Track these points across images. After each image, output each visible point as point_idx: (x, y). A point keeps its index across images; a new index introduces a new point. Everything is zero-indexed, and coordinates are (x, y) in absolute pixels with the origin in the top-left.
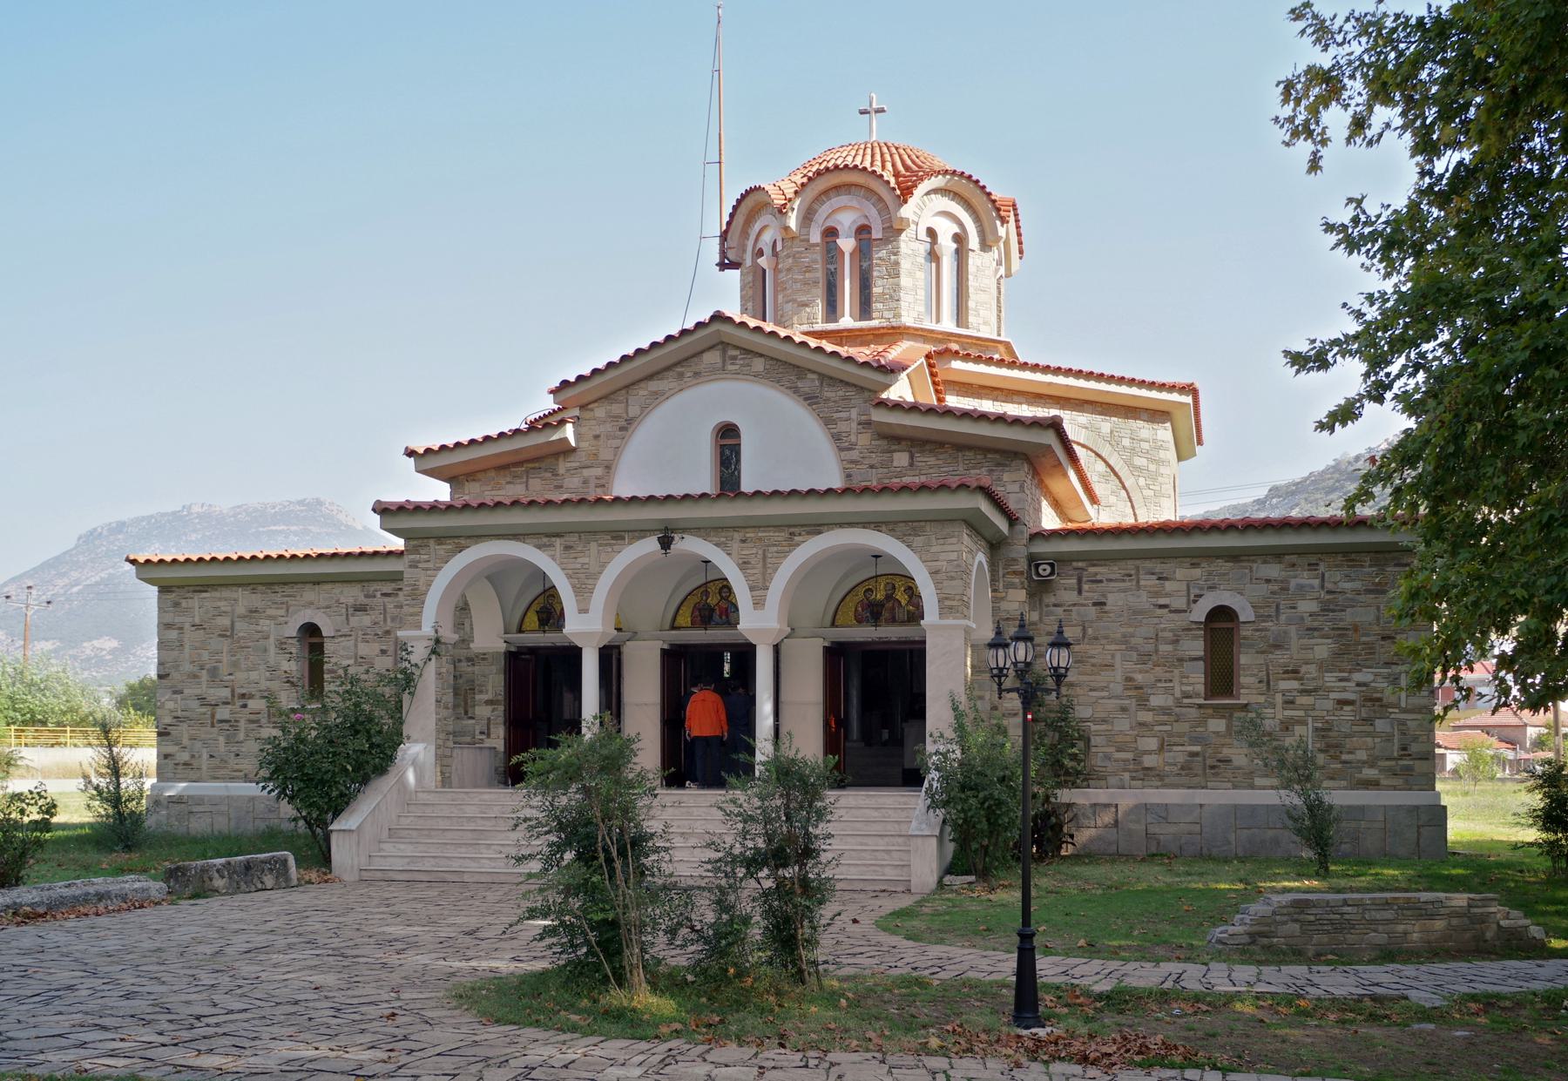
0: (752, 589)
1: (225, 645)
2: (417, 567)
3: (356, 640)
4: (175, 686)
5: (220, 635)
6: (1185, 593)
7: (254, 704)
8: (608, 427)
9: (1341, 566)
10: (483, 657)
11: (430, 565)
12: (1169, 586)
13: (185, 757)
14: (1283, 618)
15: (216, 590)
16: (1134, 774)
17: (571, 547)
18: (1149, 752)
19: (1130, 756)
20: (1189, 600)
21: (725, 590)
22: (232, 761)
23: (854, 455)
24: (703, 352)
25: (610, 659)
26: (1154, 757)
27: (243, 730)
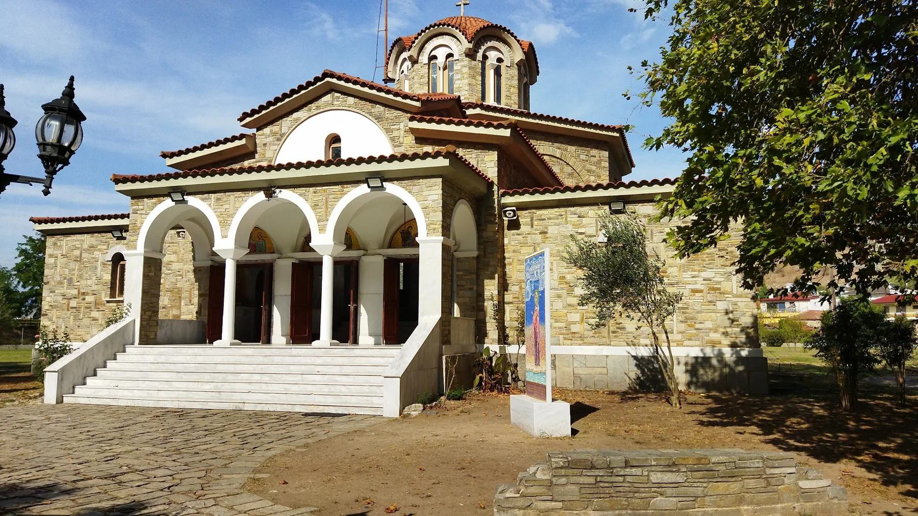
1: (77, 266)
5: (75, 261)
6: (595, 225)
7: (89, 299)
8: (271, 139)
16: (565, 336)
18: (575, 323)
19: (563, 325)
20: (597, 229)
26: (578, 325)
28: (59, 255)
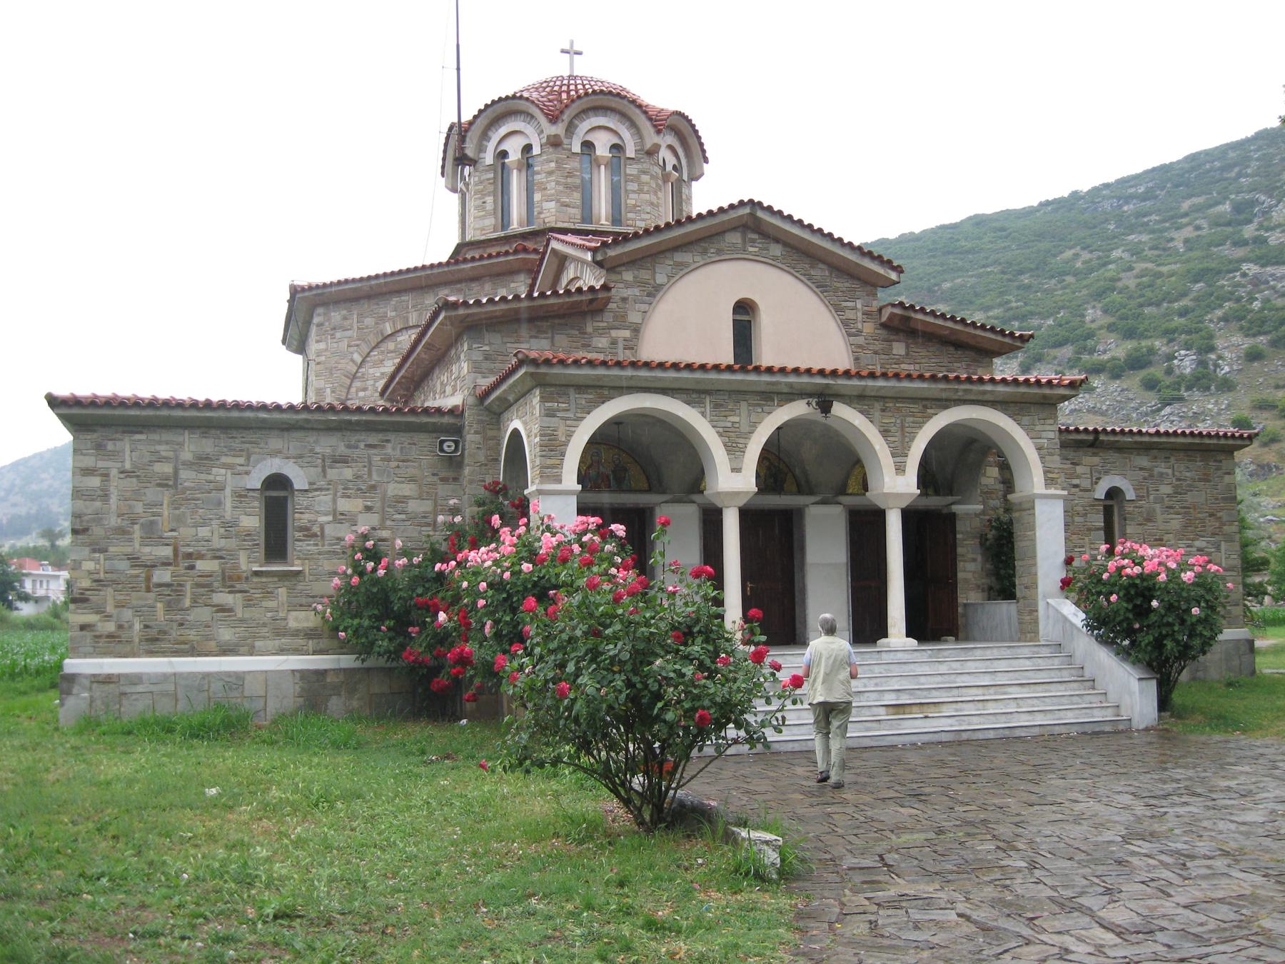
0: (893, 455)
2: (554, 416)
3: (335, 495)
4: (97, 544)
5: (159, 485)
8: (636, 291)
11: (570, 415)
12: (1079, 469)
13: (110, 627)
14: (1151, 497)
17: (722, 405)
22: (175, 633)
23: (860, 340)
24: (724, 232)
27: (189, 595)
28: (114, 472)
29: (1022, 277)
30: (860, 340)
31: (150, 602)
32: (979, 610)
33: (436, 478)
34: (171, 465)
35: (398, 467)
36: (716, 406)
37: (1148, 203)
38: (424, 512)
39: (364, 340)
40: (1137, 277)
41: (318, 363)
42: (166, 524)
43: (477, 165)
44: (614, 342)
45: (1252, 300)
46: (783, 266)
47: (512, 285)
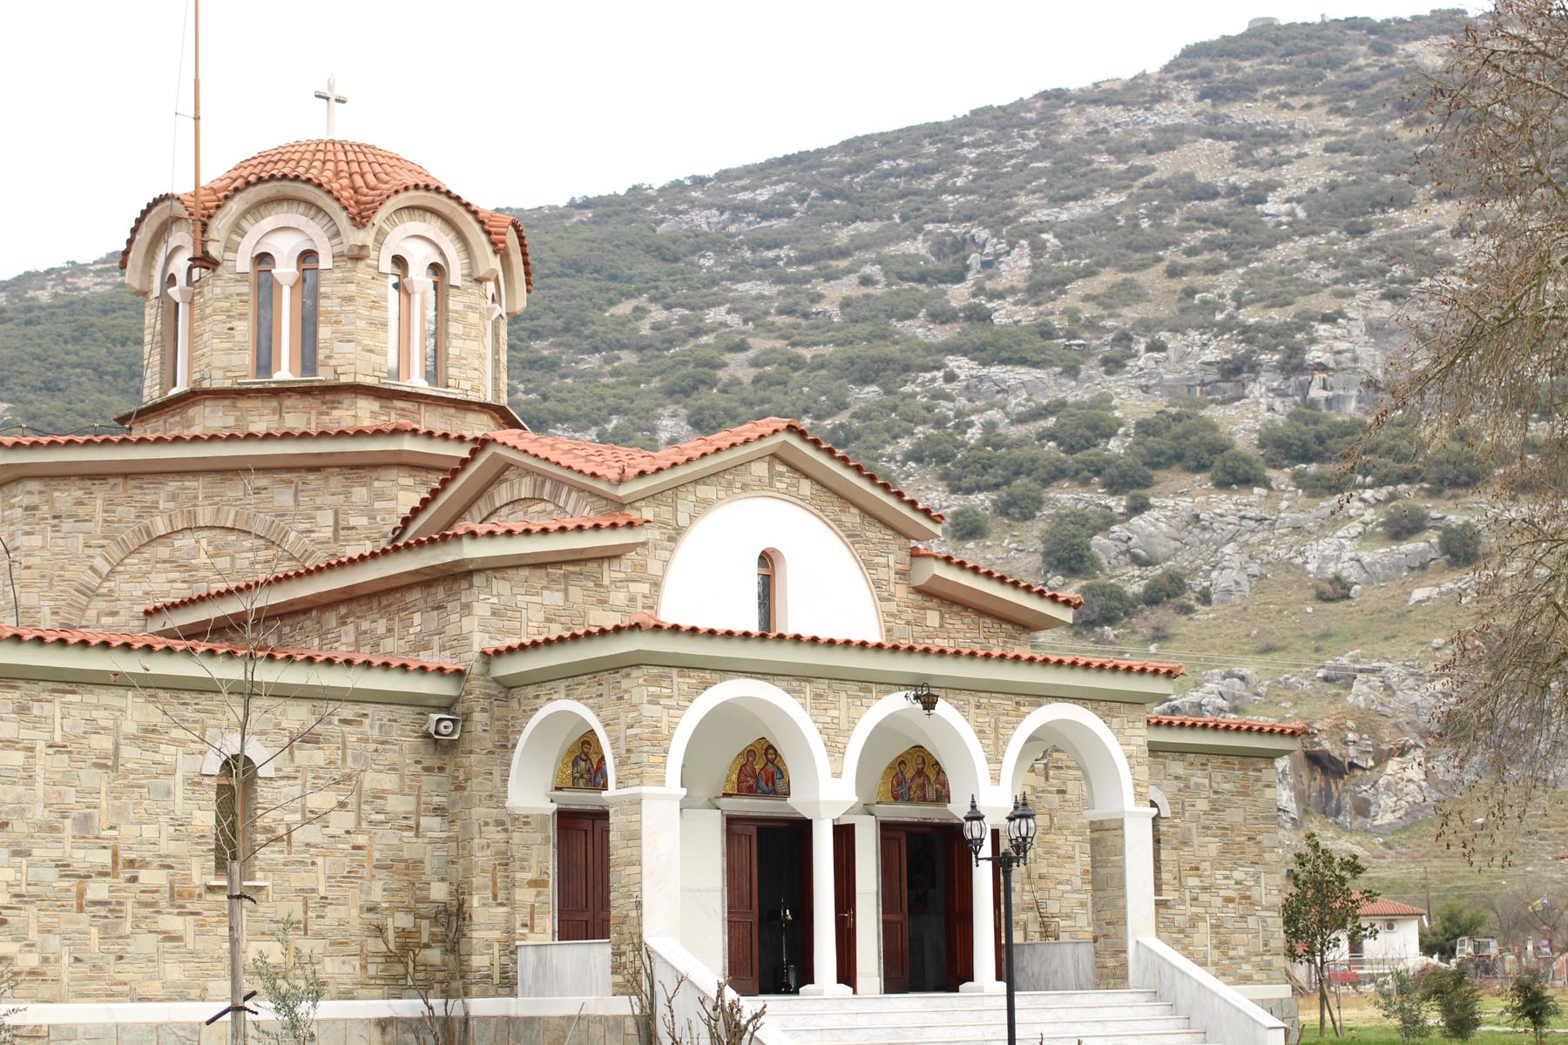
3: (304, 785)
4: (18, 844)
5: (96, 765)
7: (148, 877)
9: (1219, 767)
10: (525, 821)
11: (674, 703)
13: (30, 961)
14: (1187, 814)
15: (91, 692)
17: (822, 696)
21: (771, 751)
22: (112, 968)
25: (844, 836)
28: (41, 746)
29: (536, 345)
30: (892, 607)
31: (82, 926)
32: (1026, 954)
33: (419, 767)
34: (111, 739)
35: (376, 750)
36: (818, 696)
37: (777, 224)
38: (406, 812)
39: (112, 538)
40: (755, 363)
41: (28, 567)
42: (104, 819)
43: (220, 270)
44: (632, 599)
45: (963, 427)
46: (811, 508)
47: (376, 484)
